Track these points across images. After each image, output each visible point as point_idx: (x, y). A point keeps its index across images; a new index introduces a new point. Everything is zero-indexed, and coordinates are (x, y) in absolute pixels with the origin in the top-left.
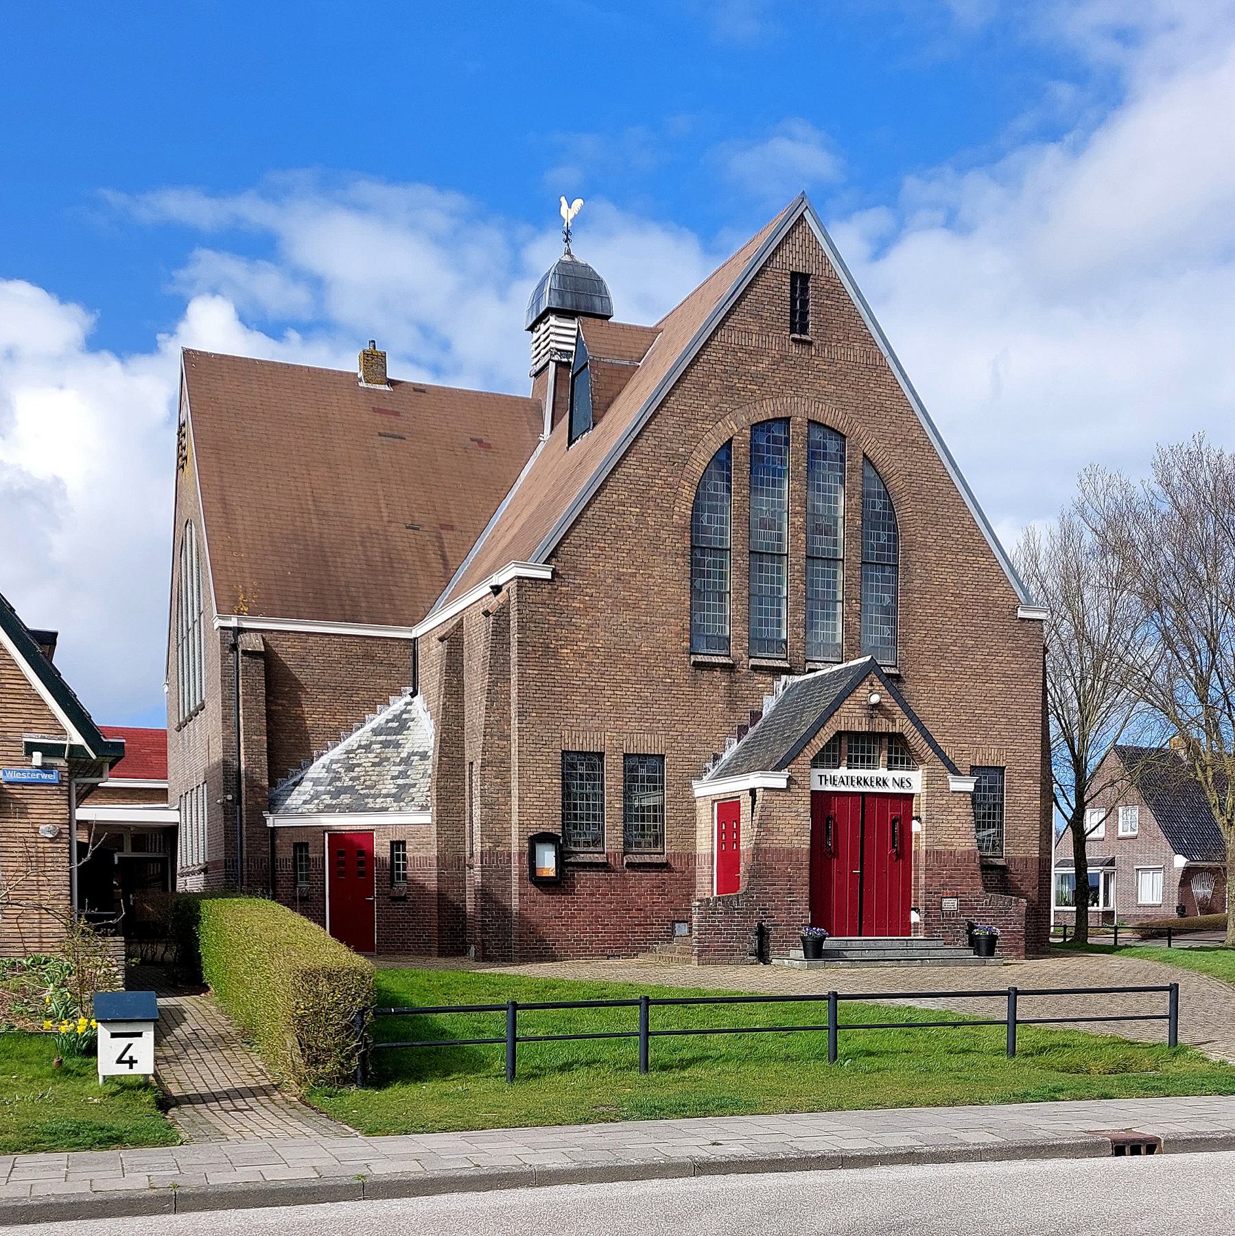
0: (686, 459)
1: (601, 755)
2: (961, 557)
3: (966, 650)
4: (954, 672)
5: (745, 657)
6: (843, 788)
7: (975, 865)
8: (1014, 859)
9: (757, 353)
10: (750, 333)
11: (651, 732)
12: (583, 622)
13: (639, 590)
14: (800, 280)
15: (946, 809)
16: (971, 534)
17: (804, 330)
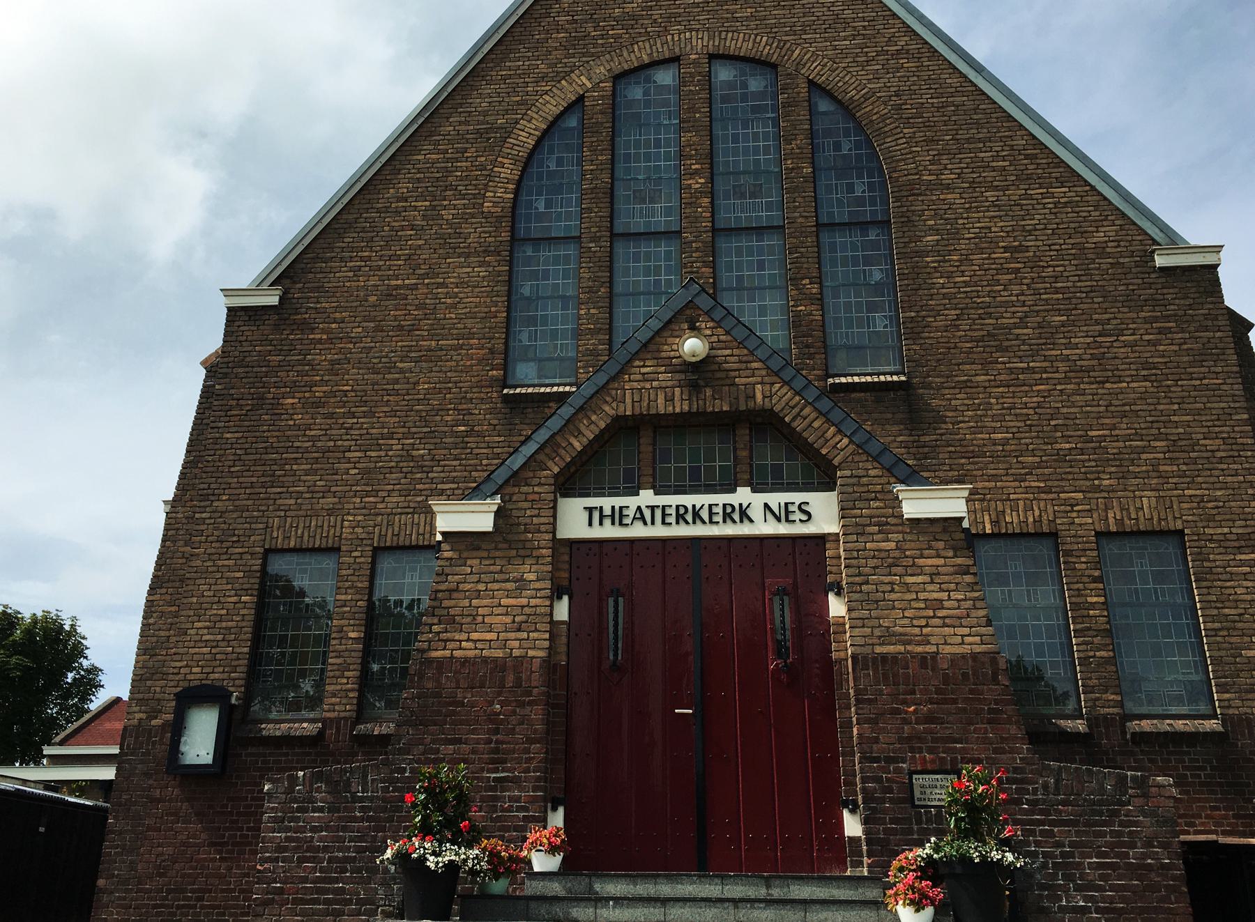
0: (508, 132)
6: (638, 531)
12: (322, 358)
15: (890, 563)
16: (1035, 157)
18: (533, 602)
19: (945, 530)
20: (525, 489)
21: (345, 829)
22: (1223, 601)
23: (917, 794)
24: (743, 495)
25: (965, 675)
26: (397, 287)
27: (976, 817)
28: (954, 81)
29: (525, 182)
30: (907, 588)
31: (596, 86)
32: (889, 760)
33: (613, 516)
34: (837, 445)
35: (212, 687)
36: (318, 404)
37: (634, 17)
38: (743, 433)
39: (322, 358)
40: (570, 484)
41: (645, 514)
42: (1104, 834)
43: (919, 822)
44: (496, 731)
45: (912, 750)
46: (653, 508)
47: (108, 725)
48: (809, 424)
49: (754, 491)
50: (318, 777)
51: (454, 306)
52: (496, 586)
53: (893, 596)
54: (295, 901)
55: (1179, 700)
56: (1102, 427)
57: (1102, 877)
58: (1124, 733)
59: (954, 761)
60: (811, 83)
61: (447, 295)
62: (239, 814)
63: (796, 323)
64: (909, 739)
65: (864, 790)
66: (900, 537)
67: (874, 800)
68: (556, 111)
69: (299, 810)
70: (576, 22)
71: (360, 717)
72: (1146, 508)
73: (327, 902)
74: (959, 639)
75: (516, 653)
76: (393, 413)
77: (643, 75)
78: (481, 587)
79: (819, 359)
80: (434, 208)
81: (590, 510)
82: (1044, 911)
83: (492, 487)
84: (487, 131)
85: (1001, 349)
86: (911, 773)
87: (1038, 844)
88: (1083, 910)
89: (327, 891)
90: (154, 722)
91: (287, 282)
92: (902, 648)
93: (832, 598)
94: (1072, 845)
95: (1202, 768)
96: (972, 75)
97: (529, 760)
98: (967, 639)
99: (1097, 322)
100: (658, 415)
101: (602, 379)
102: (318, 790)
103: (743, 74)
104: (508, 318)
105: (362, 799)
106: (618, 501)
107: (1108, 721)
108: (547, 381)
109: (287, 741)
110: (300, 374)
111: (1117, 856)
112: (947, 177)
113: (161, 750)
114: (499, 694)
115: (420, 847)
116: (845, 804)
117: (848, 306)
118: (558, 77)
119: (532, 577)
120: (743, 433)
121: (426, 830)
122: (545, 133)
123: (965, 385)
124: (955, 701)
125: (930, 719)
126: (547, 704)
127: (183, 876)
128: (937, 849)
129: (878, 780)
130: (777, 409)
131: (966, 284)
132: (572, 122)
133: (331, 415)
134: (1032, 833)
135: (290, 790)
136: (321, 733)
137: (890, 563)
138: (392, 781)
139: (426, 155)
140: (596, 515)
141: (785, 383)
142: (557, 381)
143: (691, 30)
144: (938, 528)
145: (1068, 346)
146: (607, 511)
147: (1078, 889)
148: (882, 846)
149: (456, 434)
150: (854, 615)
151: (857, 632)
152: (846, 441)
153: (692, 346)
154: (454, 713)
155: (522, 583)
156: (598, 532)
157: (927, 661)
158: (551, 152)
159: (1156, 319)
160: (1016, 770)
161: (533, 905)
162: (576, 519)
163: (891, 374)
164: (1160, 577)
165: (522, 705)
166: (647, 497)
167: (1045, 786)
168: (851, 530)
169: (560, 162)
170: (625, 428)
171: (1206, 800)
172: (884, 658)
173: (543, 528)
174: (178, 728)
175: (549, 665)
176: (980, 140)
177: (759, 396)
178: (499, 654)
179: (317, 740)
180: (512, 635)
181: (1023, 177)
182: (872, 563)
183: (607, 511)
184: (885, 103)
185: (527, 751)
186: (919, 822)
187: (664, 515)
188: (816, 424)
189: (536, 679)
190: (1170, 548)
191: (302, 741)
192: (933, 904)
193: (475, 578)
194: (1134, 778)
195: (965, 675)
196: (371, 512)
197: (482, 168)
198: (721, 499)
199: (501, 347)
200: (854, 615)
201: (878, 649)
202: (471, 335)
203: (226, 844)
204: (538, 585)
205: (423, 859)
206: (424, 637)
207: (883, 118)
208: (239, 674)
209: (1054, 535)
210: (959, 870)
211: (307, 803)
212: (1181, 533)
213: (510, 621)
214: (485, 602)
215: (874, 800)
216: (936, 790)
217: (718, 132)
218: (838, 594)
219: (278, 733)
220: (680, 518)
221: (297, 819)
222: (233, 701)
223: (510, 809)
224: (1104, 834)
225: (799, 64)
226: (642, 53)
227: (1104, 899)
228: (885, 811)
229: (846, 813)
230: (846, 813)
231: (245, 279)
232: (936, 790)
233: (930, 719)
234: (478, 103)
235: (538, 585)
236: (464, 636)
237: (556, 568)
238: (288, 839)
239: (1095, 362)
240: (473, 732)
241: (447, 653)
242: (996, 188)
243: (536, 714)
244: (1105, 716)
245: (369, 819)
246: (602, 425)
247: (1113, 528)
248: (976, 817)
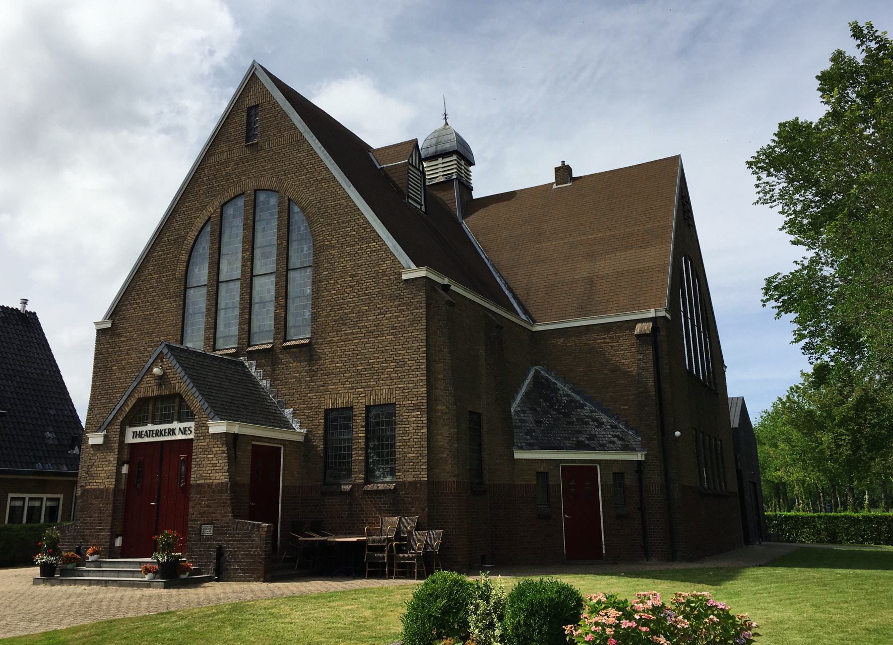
6: (146, 440)
13: (155, 323)
68: (201, 225)
82: (227, 569)
85: (343, 324)
88: (237, 569)
99: (378, 309)
101: (135, 384)
110: (119, 356)
133: (127, 373)
156: (138, 440)
159: (399, 305)
166: (150, 427)
172: (199, 485)
176: (347, 222)
181: (362, 239)
189: (111, 496)
202: (170, 334)
231: (100, 319)
234: (175, 225)
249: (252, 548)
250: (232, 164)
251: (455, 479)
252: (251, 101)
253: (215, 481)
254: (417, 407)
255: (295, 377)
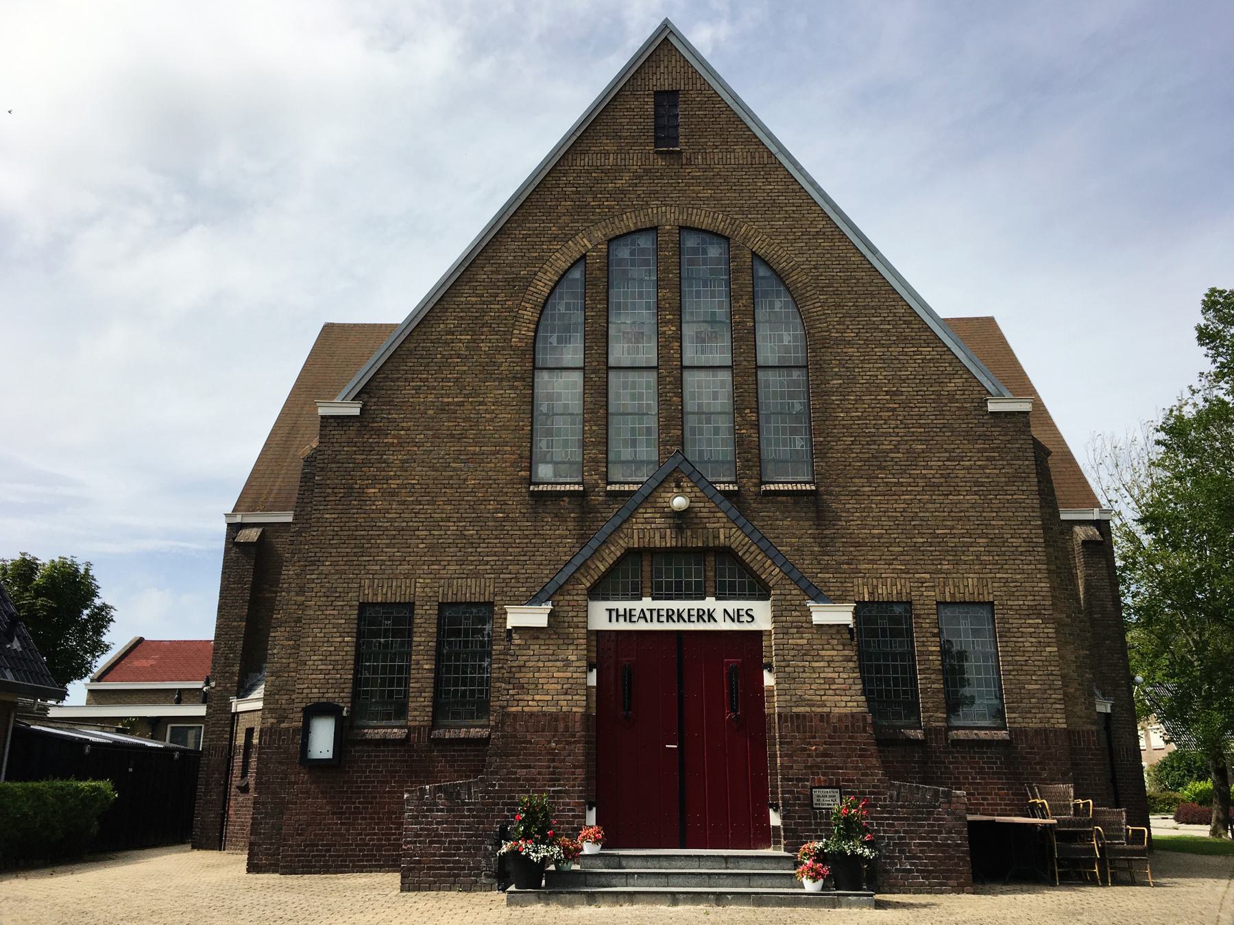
0: (529, 281)
1: (410, 606)
2: (895, 350)
3: (914, 458)
4: (901, 485)
5: (602, 483)
6: (642, 626)
7: (864, 738)
8: (1022, 732)
9: (617, 171)
10: (608, 153)
11: (476, 575)
12: (395, 458)
13: (466, 420)
14: (667, 99)
15: (804, 653)
16: (910, 323)
17: (675, 140)
18: (575, 675)
19: (838, 632)
20: (568, 598)
21: (458, 823)
22: (1015, 651)
23: (815, 801)
24: (709, 603)
25: (847, 727)
26: (448, 404)
27: (850, 828)
28: (856, 259)
29: (542, 321)
30: (814, 670)
31: (595, 249)
32: (799, 780)
33: (625, 615)
34: (771, 573)
35: (328, 704)
36: (393, 494)
37: (622, 192)
38: (711, 560)
39: (395, 458)
40: (598, 591)
41: (647, 614)
42: (924, 826)
43: (815, 818)
44: (553, 761)
45: (813, 774)
46: (651, 610)
47: (136, 663)
48: (755, 558)
49: (718, 599)
50: (439, 789)
51: (492, 420)
52: (550, 664)
53: (804, 675)
54: (429, 868)
55: (983, 716)
56: (946, 527)
57: (921, 851)
58: (947, 739)
59: (838, 780)
60: (754, 253)
61: (487, 411)
62: (352, 792)
63: (739, 442)
64: (811, 767)
65: (783, 798)
66: (809, 636)
67: (789, 805)
69: (428, 810)
70: (578, 192)
71: (434, 725)
72: (970, 586)
73: (449, 869)
74: (843, 704)
75: (564, 709)
76: (449, 502)
77: (629, 239)
78: (541, 664)
79: (755, 471)
80: (474, 341)
81: (610, 611)
83: (544, 596)
84: (513, 280)
86: (812, 788)
87: (885, 831)
88: (910, 871)
89: (449, 862)
90: (282, 725)
91: (365, 396)
92: (808, 709)
93: (765, 673)
94: (905, 832)
95: (995, 763)
96: (869, 256)
97: (574, 779)
98: (850, 704)
99: (946, 451)
100: (655, 548)
102: (440, 798)
103: (704, 242)
104: (532, 430)
105: (468, 804)
106: (629, 605)
107: (937, 731)
108: (561, 480)
109: (385, 742)
111: (931, 838)
112: (849, 335)
113: (295, 748)
114: (554, 736)
115: (526, 847)
116: (771, 806)
117: (776, 429)
118: (566, 239)
119: (573, 658)
120: (711, 560)
121: (526, 836)
122: (557, 283)
123: (856, 493)
124: (840, 743)
125: (824, 755)
126: (587, 743)
127: (315, 835)
128: (826, 845)
129: (791, 792)
130: (733, 546)
131: (859, 418)
132: (577, 274)
133: (403, 503)
134: (882, 825)
135: (421, 798)
136: (408, 735)
137: (804, 653)
138: (487, 792)
139: (467, 297)
140: (614, 614)
141: (739, 528)
142: (568, 480)
143: (666, 205)
144: (833, 631)
145: (926, 467)
146: (621, 612)
147: (907, 858)
148: (794, 837)
149: (495, 520)
150: (781, 686)
151: (782, 698)
152: (777, 570)
153: (679, 502)
154: (525, 748)
155: (567, 663)
157: (824, 718)
158: (561, 298)
159: (985, 450)
160: (874, 787)
161: (589, 877)
162: (601, 616)
163: (806, 483)
164: (976, 633)
165: (569, 743)
166: (647, 603)
167: (891, 797)
168: (779, 631)
169: (568, 307)
170: (632, 554)
171: (996, 784)
172: (798, 715)
173: (580, 625)
174: (305, 733)
175: (586, 716)
177: (722, 537)
178: (553, 709)
179: (404, 742)
180: (562, 697)
182: (792, 653)
183: (621, 612)
184: (807, 274)
185: (574, 773)
186: (815, 818)
187: (659, 615)
188: (759, 558)
190: (984, 613)
191: (394, 742)
192: (823, 876)
193: (536, 658)
194: (943, 792)
195: (847, 727)
196: (436, 577)
197: (510, 310)
198: (695, 605)
199: (528, 453)
200: (781, 686)
201: (795, 710)
202: (506, 444)
203: (344, 813)
204: (578, 664)
205: (528, 855)
206: (504, 698)
207: (805, 285)
208: (347, 693)
209: (910, 603)
210: (838, 858)
211: (432, 806)
212: (992, 603)
213: (558, 687)
214: (544, 675)
215: (789, 805)
216: (829, 800)
217: (685, 289)
218: (770, 671)
219: (378, 737)
220: (669, 617)
221: (426, 817)
222: (345, 714)
223: (563, 811)
224: (924, 826)
225: (746, 238)
226: (630, 222)
227: (921, 865)
228: (795, 812)
229: (771, 811)
230: (771, 811)
232: (829, 800)
233: (824, 755)
234: (507, 255)
235: (578, 664)
236: (530, 698)
237: (588, 650)
238: (421, 829)
239: (943, 480)
240: (539, 760)
241: (519, 709)
242: (883, 346)
243: (579, 749)
244: (935, 729)
245: (474, 817)
246: (619, 554)
247: (948, 600)
248: (850, 828)
249: (940, 832)
250: (627, 176)
251: (1094, 728)
252: (664, 82)
253: (836, 710)
254: (1035, 611)
255: (791, 545)
